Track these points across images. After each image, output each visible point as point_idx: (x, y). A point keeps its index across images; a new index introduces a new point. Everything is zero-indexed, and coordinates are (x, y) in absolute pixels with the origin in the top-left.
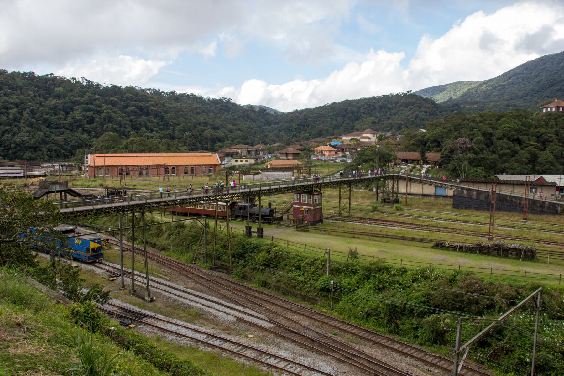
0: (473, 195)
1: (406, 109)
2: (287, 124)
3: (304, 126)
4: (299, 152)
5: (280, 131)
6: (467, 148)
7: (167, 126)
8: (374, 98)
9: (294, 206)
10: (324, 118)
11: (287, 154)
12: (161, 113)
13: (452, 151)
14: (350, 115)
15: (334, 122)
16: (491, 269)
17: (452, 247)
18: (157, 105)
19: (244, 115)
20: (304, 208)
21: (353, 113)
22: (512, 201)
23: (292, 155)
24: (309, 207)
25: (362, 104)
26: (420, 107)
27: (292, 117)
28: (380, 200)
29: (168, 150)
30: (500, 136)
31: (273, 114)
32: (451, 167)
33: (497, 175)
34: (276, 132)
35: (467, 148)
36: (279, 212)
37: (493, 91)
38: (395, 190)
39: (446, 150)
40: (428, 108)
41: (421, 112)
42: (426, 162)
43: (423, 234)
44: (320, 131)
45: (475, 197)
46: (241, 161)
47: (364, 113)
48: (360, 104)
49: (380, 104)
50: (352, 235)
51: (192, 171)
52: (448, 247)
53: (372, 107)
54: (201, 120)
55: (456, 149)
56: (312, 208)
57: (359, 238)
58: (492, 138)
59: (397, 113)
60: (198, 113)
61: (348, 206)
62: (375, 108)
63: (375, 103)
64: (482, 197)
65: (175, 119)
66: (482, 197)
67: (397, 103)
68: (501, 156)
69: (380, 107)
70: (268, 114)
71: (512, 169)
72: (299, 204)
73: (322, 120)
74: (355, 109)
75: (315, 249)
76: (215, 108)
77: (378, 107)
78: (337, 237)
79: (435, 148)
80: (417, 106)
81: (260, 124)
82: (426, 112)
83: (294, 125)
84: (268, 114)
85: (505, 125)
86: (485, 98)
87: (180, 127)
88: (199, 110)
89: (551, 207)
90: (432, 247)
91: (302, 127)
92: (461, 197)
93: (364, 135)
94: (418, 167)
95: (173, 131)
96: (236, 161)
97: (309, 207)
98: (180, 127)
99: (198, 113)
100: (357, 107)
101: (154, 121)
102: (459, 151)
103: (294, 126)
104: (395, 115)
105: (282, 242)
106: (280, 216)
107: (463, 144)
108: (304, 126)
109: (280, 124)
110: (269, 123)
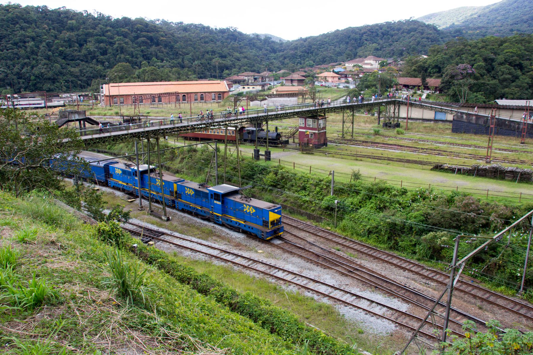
0: (472, 119)
1: (408, 36)
2: (292, 52)
3: (308, 53)
4: (304, 78)
5: (285, 58)
6: (467, 73)
7: (176, 55)
8: (377, 25)
9: (300, 130)
10: (327, 45)
11: (292, 81)
12: (170, 42)
13: (453, 77)
14: (353, 42)
15: (338, 49)
17: (451, 170)
18: (166, 35)
19: (250, 44)
20: (309, 132)
21: (356, 40)
22: (511, 125)
23: (296, 82)
24: (314, 131)
25: (365, 31)
26: (422, 34)
27: (297, 45)
28: (381, 124)
29: (178, 79)
30: (502, 62)
31: (278, 42)
32: (451, 92)
33: (497, 100)
34: (281, 59)
35: (467, 73)
37: (497, 15)
39: (447, 75)
40: (431, 34)
41: (423, 38)
42: (427, 88)
43: (423, 157)
44: (324, 58)
45: (474, 122)
46: (248, 88)
47: (366, 40)
48: (362, 31)
49: (382, 31)
50: (354, 158)
51: (202, 98)
52: (447, 169)
53: (374, 34)
54: (209, 48)
55: (457, 75)
56: (317, 132)
57: (361, 160)
58: (494, 64)
59: (399, 39)
60: (206, 42)
61: (351, 130)
62: (377, 35)
63: (377, 29)
64: (481, 122)
65: (184, 48)
66: (481, 122)
67: (399, 30)
68: (501, 82)
69: (382, 33)
70: (273, 42)
71: (512, 94)
72: (305, 128)
73: (326, 48)
74: (358, 36)
75: (319, 171)
76: (222, 37)
77: (380, 34)
78: (341, 160)
79: (436, 74)
80: (419, 32)
81: (265, 52)
82: (428, 38)
83: (299, 52)
84: (273, 42)
85: (508, 51)
86: (488, 23)
87: (189, 56)
88: (207, 40)
90: (431, 170)
91: (306, 54)
92: (460, 121)
93: (366, 62)
94: (419, 92)
95: (183, 60)
97: (314, 131)
98: (189, 56)
99: (206, 42)
100: (360, 34)
101: (164, 50)
102: (460, 77)
103: (299, 53)
104: (397, 41)
106: (286, 139)
107: (464, 70)
108: (308, 53)
109: (285, 52)
110: (274, 51)
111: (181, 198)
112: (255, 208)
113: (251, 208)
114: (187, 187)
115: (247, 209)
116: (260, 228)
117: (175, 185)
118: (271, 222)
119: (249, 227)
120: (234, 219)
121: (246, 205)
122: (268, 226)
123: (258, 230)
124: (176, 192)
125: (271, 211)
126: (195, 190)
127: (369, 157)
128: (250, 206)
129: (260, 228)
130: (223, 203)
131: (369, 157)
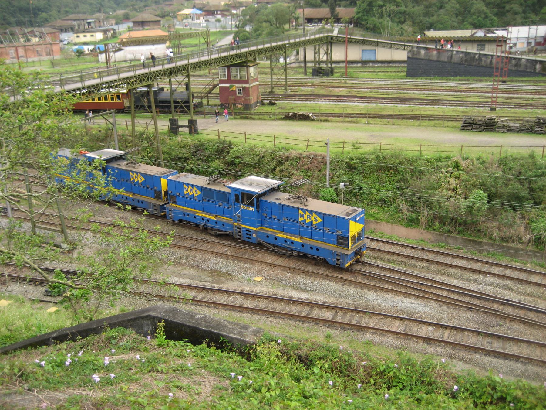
4: (158, 19)
16: (344, 142)
28: (310, 71)
36: (198, 97)
38: (317, 59)
42: (338, 20)
46: (85, 36)
57: (326, 121)
61: (283, 82)
72: (229, 81)
89: (529, 65)
92: (417, 59)
96: (78, 36)
105: (236, 135)
111: (174, 202)
112: (144, 175)
113: (139, 175)
114: (187, 185)
115: (304, 218)
116: (153, 201)
117: (164, 181)
118: (352, 237)
119: (311, 248)
120: (281, 235)
121: (133, 172)
122: (346, 246)
123: (330, 252)
124: (166, 193)
125: (351, 219)
126: (201, 189)
127: (339, 115)
128: (137, 173)
129: (332, 247)
130: (258, 207)
131: (339, 115)
